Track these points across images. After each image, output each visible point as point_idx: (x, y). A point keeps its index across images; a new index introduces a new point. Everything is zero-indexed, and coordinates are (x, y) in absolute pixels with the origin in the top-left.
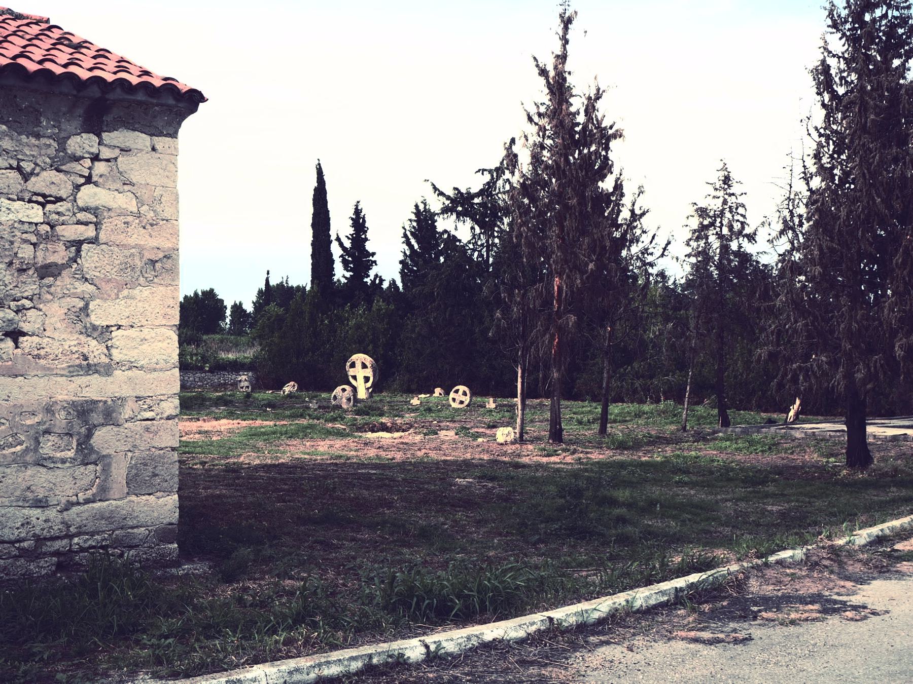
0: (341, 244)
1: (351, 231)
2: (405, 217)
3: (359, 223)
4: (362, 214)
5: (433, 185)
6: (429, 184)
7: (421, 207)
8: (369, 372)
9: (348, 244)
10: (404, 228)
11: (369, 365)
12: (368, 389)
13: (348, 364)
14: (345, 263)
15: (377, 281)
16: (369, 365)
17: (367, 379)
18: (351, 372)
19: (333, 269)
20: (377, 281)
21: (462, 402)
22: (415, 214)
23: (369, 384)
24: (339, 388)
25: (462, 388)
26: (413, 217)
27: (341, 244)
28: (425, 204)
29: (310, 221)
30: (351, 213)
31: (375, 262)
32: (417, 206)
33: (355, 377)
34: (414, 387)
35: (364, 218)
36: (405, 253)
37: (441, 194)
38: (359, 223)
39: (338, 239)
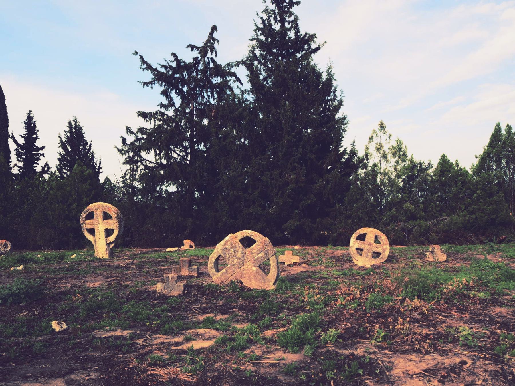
0: (15, 141)
1: (25, 132)
2: (62, 130)
3: (30, 125)
4: (33, 120)
5: (141, 57)
6: (138, 57)
7: (73, 123)
8: (113, 224)
9: (21, 141)
10: (59, 137)
11: (114, 215)
12: (108, 244)
13: (83, 215)
14: (18, 154)
15: (46, 169)
16: (114, 215)
17: (109, 232)
18: (88, 224)
19: (10, 158)
20: (46, 169)
21: (376, 255)
22: (69, 127)
23: (112, 238)
24: (233, 239)
25: (370, 232)
26: (68, 129)
27: (15, 141)
28: (76, 122)
29: (5, 94)
30: (25, 119)
31: (43, 155)
32: (70, 123)
33: (92, 232)
34: (380, 228)
35: (34, 123)
36: (60, 154)
37: (149, 67)
38: (30, 125)
39: (13, 137)
